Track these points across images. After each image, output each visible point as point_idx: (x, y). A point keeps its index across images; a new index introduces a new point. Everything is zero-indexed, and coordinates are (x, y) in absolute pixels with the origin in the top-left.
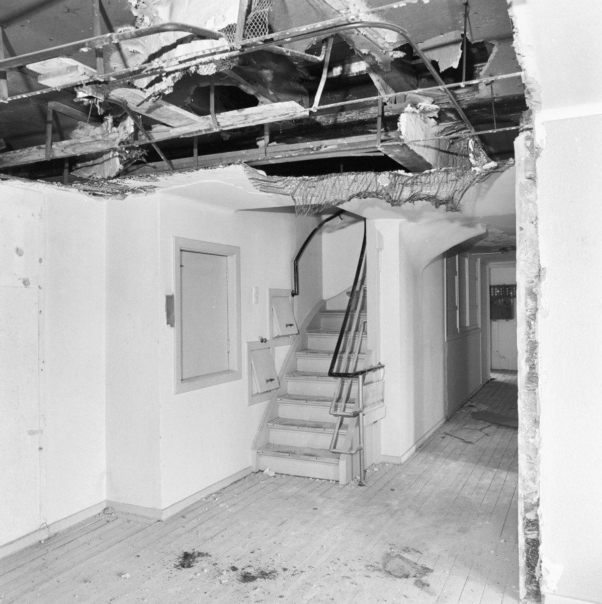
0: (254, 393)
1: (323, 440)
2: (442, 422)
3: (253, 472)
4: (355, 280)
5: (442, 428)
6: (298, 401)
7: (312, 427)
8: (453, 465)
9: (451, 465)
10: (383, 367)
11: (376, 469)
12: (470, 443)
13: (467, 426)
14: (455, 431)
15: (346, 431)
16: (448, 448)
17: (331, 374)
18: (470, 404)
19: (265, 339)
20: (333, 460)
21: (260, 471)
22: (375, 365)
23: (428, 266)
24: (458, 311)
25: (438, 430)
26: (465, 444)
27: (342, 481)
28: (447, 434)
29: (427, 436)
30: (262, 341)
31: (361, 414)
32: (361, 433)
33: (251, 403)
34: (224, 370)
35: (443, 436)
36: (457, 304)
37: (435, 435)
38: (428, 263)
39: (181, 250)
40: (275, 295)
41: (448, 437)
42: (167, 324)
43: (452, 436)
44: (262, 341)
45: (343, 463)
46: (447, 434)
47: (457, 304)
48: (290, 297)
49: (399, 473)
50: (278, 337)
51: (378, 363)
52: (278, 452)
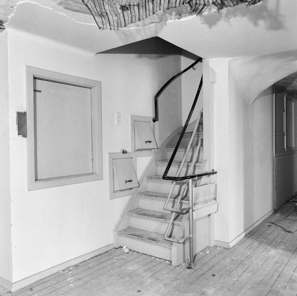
0: (115, 190)
1: (164, 227)
2: (270, 214)
3: (114, 248)
4: (192, 106)
5: (270, 218)
6: (151, 197)
7: (157, 217)
8: (273, 252)
9: (270, 253)
10: (216, 173)
11: (208, 252)
12: (290, 232)
13: (289, 217)
14: (280, 220)
15: (181, 222)
16: (271, 236)
17: (165, 177)
18: (294, 200)
19: (126, 151)
20: (167, 246)
21: (120, 247)
22: (208, 170)
23: (256, 99)
24: (285, 137)
25: (267, 219)
26: (285, 232)
27: (174, 263)
28: (273, 223)
29: (256, 225)
30: (123, 153)
31: (191, 210)
32: (191, 226)
33: (112, 198)
34: (89, 173)
35: (270, 224)
36: (285, 131)
37: (264, 223)
38: (256, 96)
39: (35, 78)
40: (136, 122)
41: (273, 226)
42: (19, 134)
43: (276, 225)
44: (123, 153)
45: (175, 248)
46: (273, 223)
47: (285, 131)
48: (152, 122)
49: (225, 258)
50: (139, 150)
51: (211, 170)
52: (131, 235)
